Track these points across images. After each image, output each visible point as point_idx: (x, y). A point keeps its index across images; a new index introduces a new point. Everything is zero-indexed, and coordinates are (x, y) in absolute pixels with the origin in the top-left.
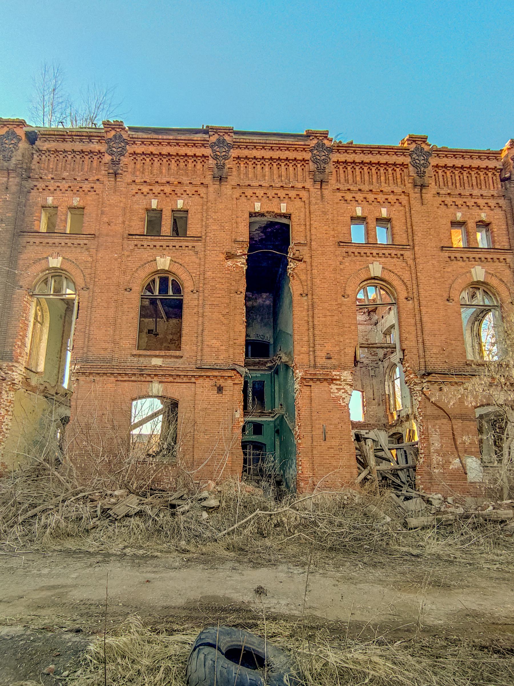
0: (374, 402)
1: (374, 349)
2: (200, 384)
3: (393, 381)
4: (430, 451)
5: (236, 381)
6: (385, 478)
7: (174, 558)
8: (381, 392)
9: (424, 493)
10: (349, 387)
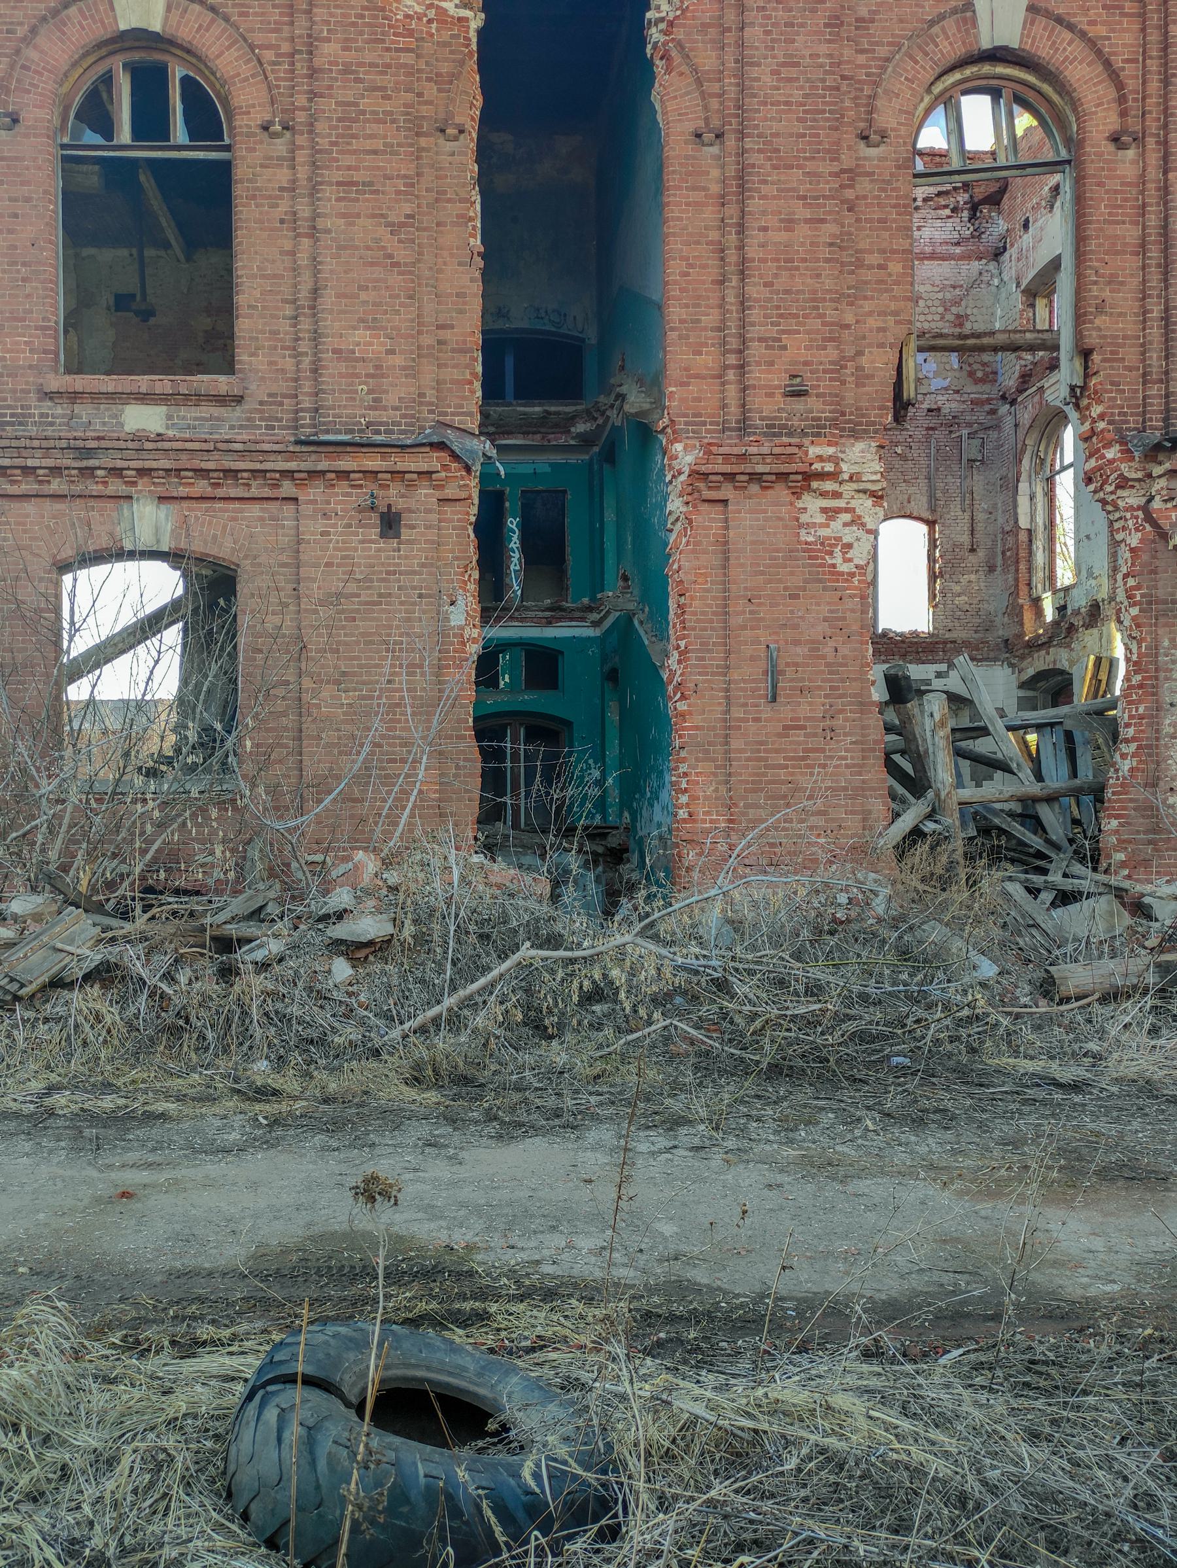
0: (972, 559)
1: (986, 357)
2: (314, 502)
3: (1050, 481)
4: (1157, 731)
5: (450, 492)
6: (985, 831)
7: (225, 1117)
8: (1000, 521)
9: (1129, 877)
10: (869, 502)
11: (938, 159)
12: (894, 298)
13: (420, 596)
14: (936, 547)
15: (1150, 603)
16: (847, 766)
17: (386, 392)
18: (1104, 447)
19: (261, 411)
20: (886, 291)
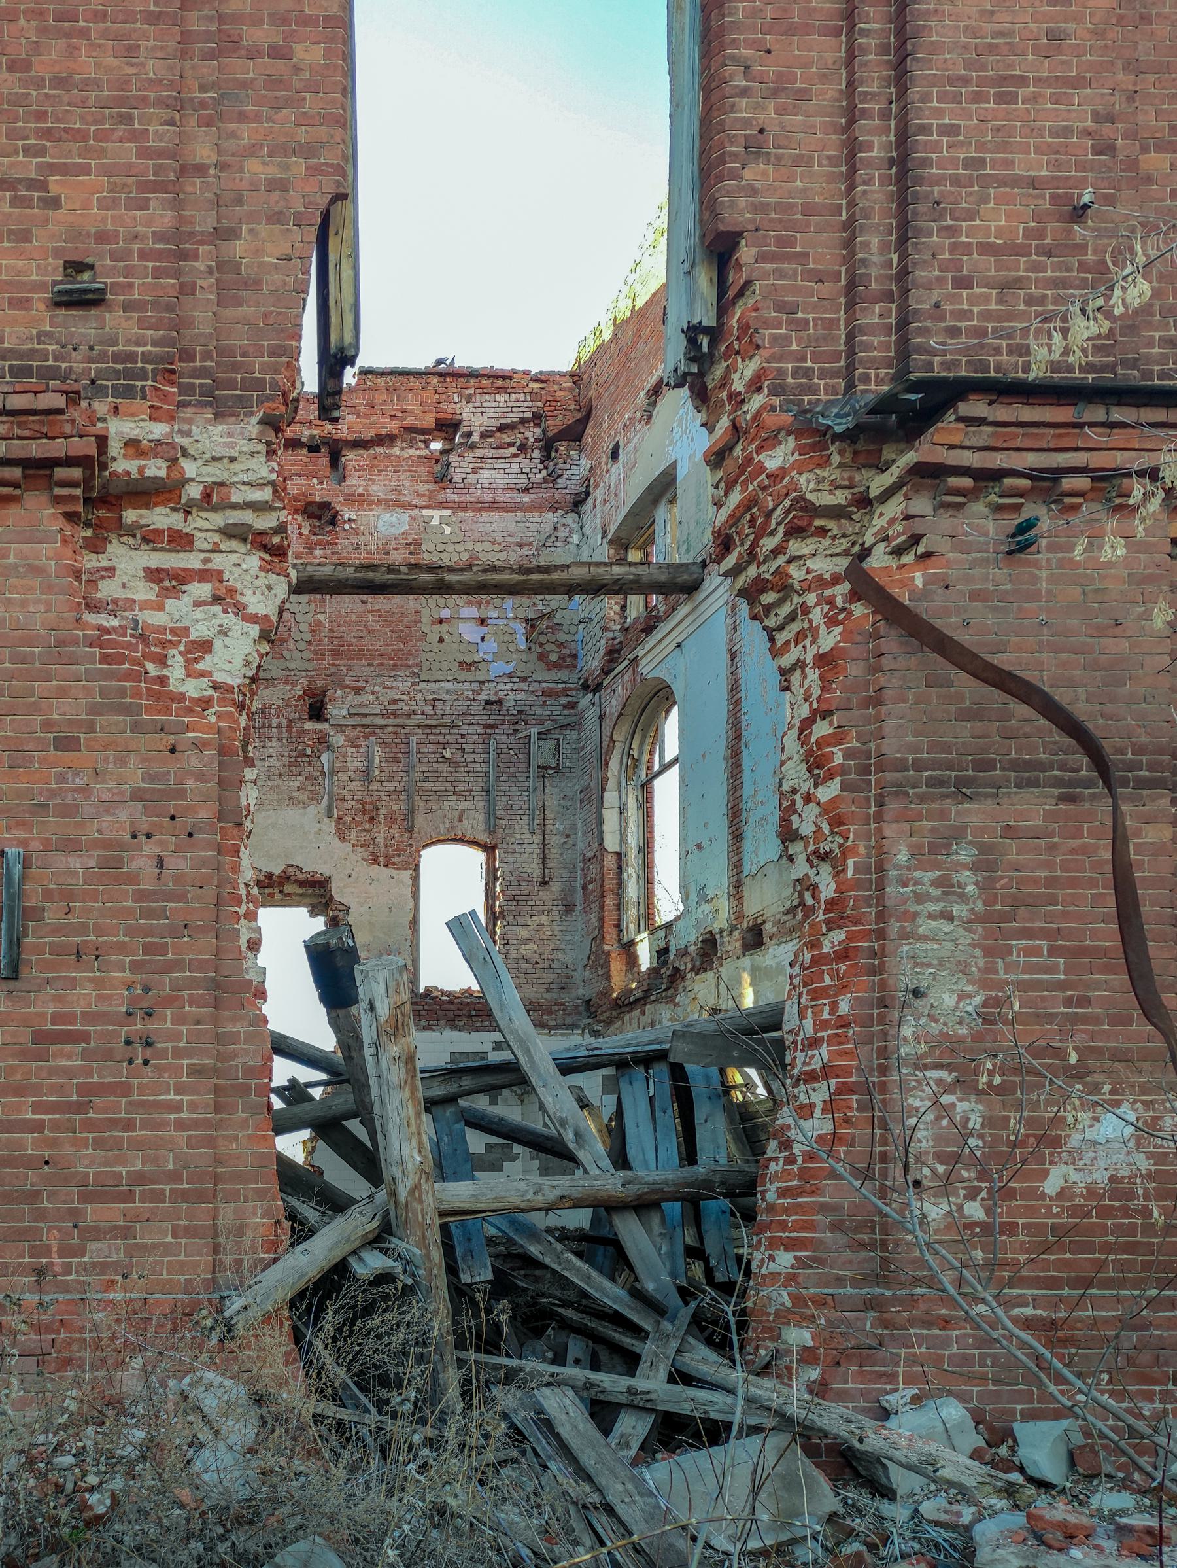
0: (544, 895)
3: (646, 788)
4: (883, 1052)
8: (581, 845)
10: (253, 561)
11: (500, 383)
12: (305, 120)
14: (496, 879)
15: (865, 770)
16: (181, 1125)
18: (760, 449)
20: (288, 103)
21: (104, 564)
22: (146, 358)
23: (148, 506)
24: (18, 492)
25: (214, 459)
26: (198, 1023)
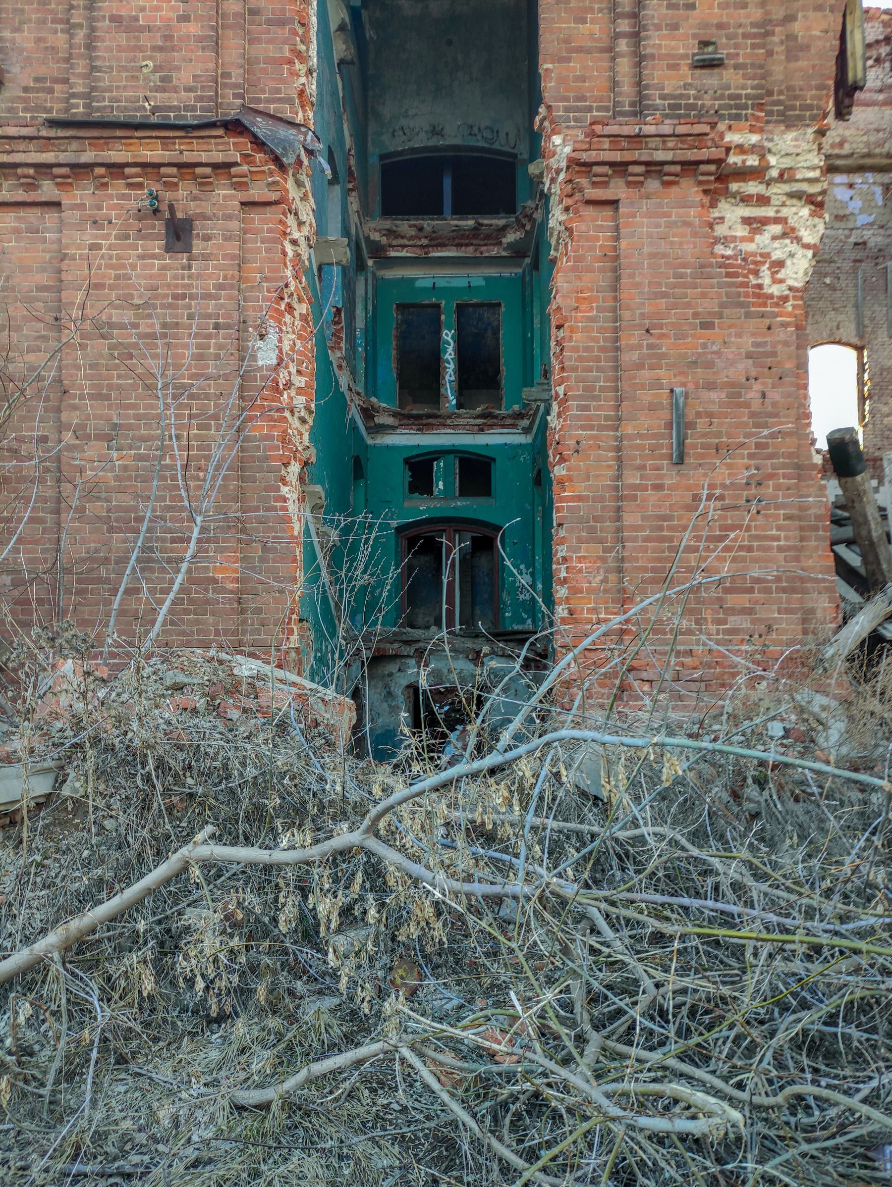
2: (82, 207)
5: (257, 192)
10: (805, 211)
13: (217, 326)
14: (864, 371)
16: (780, 549)
17: (178, 69)
19: (26, 100)
21: (716, 215)
22: (748, 97)
23: (744, 181)
24: (677, 179)
25: (787, 154)
26: (788, 489)
